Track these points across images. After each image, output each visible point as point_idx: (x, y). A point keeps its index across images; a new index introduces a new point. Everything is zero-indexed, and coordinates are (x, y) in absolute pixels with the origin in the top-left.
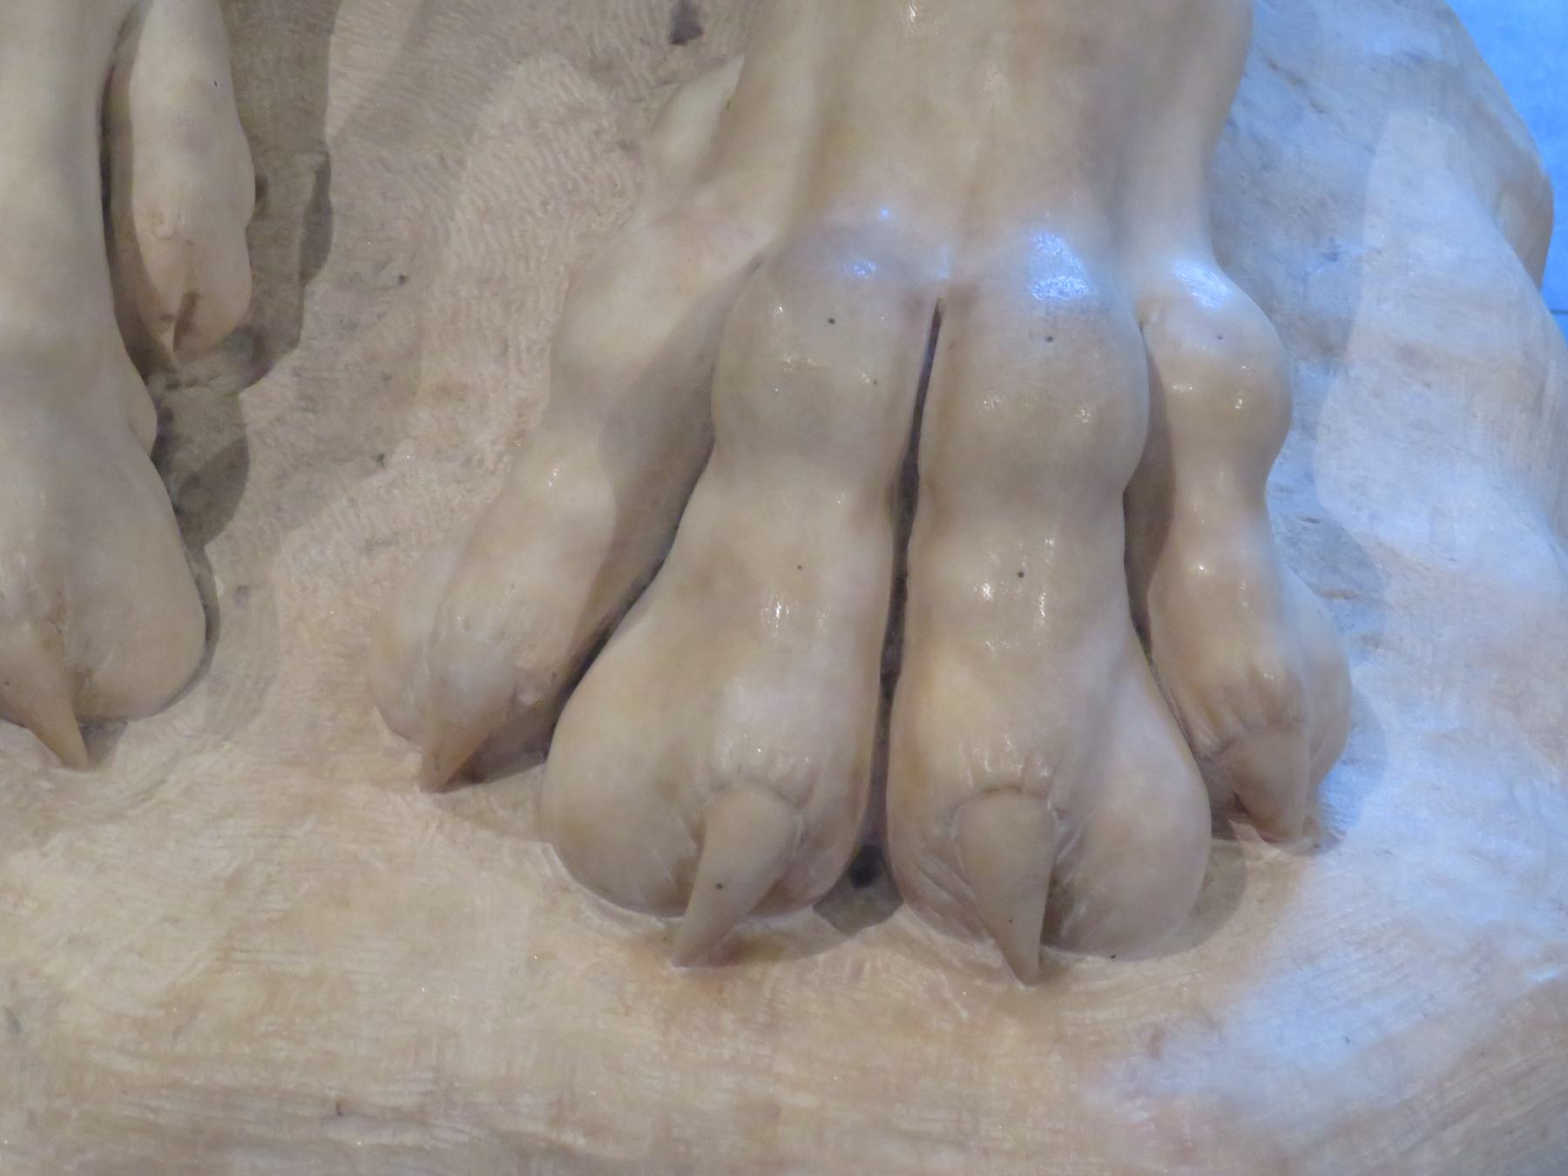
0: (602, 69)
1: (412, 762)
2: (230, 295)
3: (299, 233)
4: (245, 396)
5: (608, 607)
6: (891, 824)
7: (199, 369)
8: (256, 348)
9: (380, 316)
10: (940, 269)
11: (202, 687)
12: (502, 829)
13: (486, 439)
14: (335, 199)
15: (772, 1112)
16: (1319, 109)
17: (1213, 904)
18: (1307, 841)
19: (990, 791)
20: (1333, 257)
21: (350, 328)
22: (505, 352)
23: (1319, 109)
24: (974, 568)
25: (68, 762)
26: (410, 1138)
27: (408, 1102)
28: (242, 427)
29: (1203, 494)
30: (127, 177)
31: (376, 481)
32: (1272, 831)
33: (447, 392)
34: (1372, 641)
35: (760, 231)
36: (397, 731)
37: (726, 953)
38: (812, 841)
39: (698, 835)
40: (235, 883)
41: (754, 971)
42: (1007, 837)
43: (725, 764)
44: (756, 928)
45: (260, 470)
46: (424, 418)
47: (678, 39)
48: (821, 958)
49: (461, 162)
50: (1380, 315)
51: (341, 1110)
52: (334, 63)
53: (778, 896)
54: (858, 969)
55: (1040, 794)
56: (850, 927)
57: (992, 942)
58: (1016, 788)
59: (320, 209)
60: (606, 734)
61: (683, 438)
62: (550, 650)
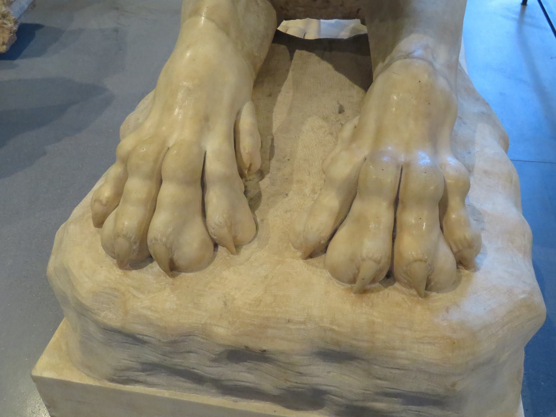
0: (325, 119)
1: (299, 254)
2: (257, 164)
3: (269, 151)
4: (260, 182)
5: (337, 224)
6: (395, 267)
7: (251, 177)
8: (262, 174)
9: (285, 167)
10: (402, 159)
11: (256, 239)
12: (317, 267)
13: (307, 191)
14: (275, 145)
15: (373, 323)
16: (465, 123)
17: (456, 282)
18: (473, 269)
19: (416, 261)
20: (470, 153)
21: (279, 169)
22: (309, 174)
23: (465, 123)
24: (410, 217)
25: (232, 253)
26: (303, 327)
27: (302, 320)
28: (260, 189)
29: (454, 202)
30: (239, 143)
31: (286, 199)
32: (466, 267)
33: (298, 182)
34: (483, 229)
35: (365, 152)
36: (295, 248)
37: (363, 291)
38: (381, 270)
39: (358, 269)
40: (266, 277)
41: (369, 295)
42: (419, 270)
43: (364, 255)
44: (368, 287)
45: (264, 197)
46: (295, 186)
47: (340, 112)
48: (381, 292)
49: (299, 137)
50: (480, 164)
51: (289, 321)
52: (274, 119)
53: (373, 281)
54: (388, 294)
55: (426, 262)
56: (386, 287)
57: (414, 289)
58: (421, 260)
59: (272, 147)
60: (339, 249)
61: (352, 192)
62: (326, 233)
